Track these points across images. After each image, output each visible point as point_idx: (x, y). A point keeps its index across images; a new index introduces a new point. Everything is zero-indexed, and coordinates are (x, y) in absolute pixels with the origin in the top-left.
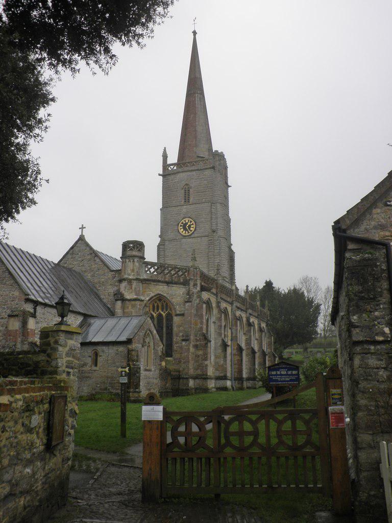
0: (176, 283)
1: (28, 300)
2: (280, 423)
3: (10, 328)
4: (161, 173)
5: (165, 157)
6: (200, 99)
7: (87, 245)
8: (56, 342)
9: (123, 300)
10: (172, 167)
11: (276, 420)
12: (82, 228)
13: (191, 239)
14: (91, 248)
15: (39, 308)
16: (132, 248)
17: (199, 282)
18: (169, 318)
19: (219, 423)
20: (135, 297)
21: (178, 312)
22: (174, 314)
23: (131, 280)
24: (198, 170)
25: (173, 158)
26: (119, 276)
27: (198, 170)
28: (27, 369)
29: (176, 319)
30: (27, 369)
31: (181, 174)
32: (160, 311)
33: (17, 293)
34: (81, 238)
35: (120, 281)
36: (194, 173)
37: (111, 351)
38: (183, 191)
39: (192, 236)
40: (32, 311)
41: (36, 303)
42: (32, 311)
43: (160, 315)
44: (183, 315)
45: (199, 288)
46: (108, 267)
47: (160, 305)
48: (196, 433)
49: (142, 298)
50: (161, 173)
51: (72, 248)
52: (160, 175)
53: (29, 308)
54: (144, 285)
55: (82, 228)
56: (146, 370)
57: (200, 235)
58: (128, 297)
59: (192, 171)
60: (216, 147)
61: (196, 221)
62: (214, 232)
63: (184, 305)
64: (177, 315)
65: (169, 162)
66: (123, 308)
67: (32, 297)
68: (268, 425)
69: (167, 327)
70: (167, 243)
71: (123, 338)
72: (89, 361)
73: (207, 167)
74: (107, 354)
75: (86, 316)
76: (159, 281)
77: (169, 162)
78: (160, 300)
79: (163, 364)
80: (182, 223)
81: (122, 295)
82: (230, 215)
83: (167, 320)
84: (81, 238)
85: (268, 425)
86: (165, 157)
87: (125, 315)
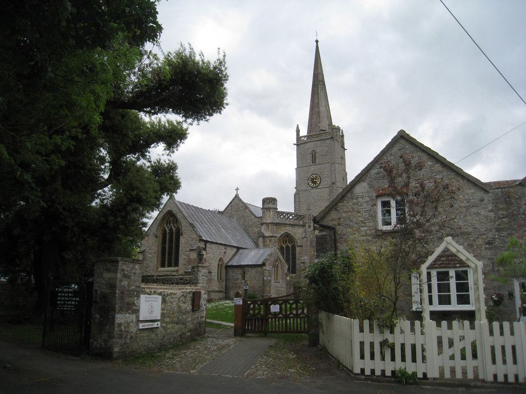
0: (297, 225)
1: (201, 240)
2: (291, 305)
3: (191, 257)
4: (295, 143)
5: (298, 131)
6: (322, 88)
7: (240, 200)
8: (198, 271)
9: (264, 237)
10: (303, 138)
11: (289, 303)
12: (237, 189)
13: (317, 190)
14: (243, 202)
15: (208, 245)
16: (269, 202)
17: (312, 225)
18: (294, 248)
19: (266, 305)
20: (271, 234)
21: (299, 244)
22: (296, 246)
23: (268, 223)
24: (321, 140)
25: (304, 132)
26: (261, 222)
27: (321, 140)
28: (515, 386)
29: (298, 249)
30: (515, 386)
31: (309, 143)
32: (287, 243)
33: (194, 236)
34: (237, 197)
35: (262, 224)
36: (319, 142)
37: (253, 271)
38: (311, 155)
39: (319, 187)
40: (204, 247)
41: (206, 242)
42: (204, 247)
43: (288, 246)
44: (302, 246)
45: (312, 228)
46: (254, 215)
47: (287, 239)
48: (269, 309)
49: (276, 235)
50: (295, 143)
51: (231, 203)
52: (294, 144)
53: (202, 245)
54: (278, 227)
55: (237, 189)
56: (275, 282)
57: (324, 186)
58: (267, 235)
59: (316, 141)
60: (335, 123)
61: (308, 185)
62: (333, 184)
63: (303, 239)
64: (298, 246)
65: (301, 135)
66: (264, 242)
67: (204, 238)
68: (286, 306)
69: (293, 255)
70: (301, 193)
71: (260, 263)
72: (240, 276)
73: (327, 138)
74: (251, 273)
75: (238, 248)
76: (286, 224)
77: (301, 135)
78: (287, 236)
79: (288, 278)
80: (311, 178)
81: (263, 234)
82: (347, 170)
83: (292, 249)
84: (237, 197)
85: (286, 306)
86: (298, 131)
87: (265, 246)
